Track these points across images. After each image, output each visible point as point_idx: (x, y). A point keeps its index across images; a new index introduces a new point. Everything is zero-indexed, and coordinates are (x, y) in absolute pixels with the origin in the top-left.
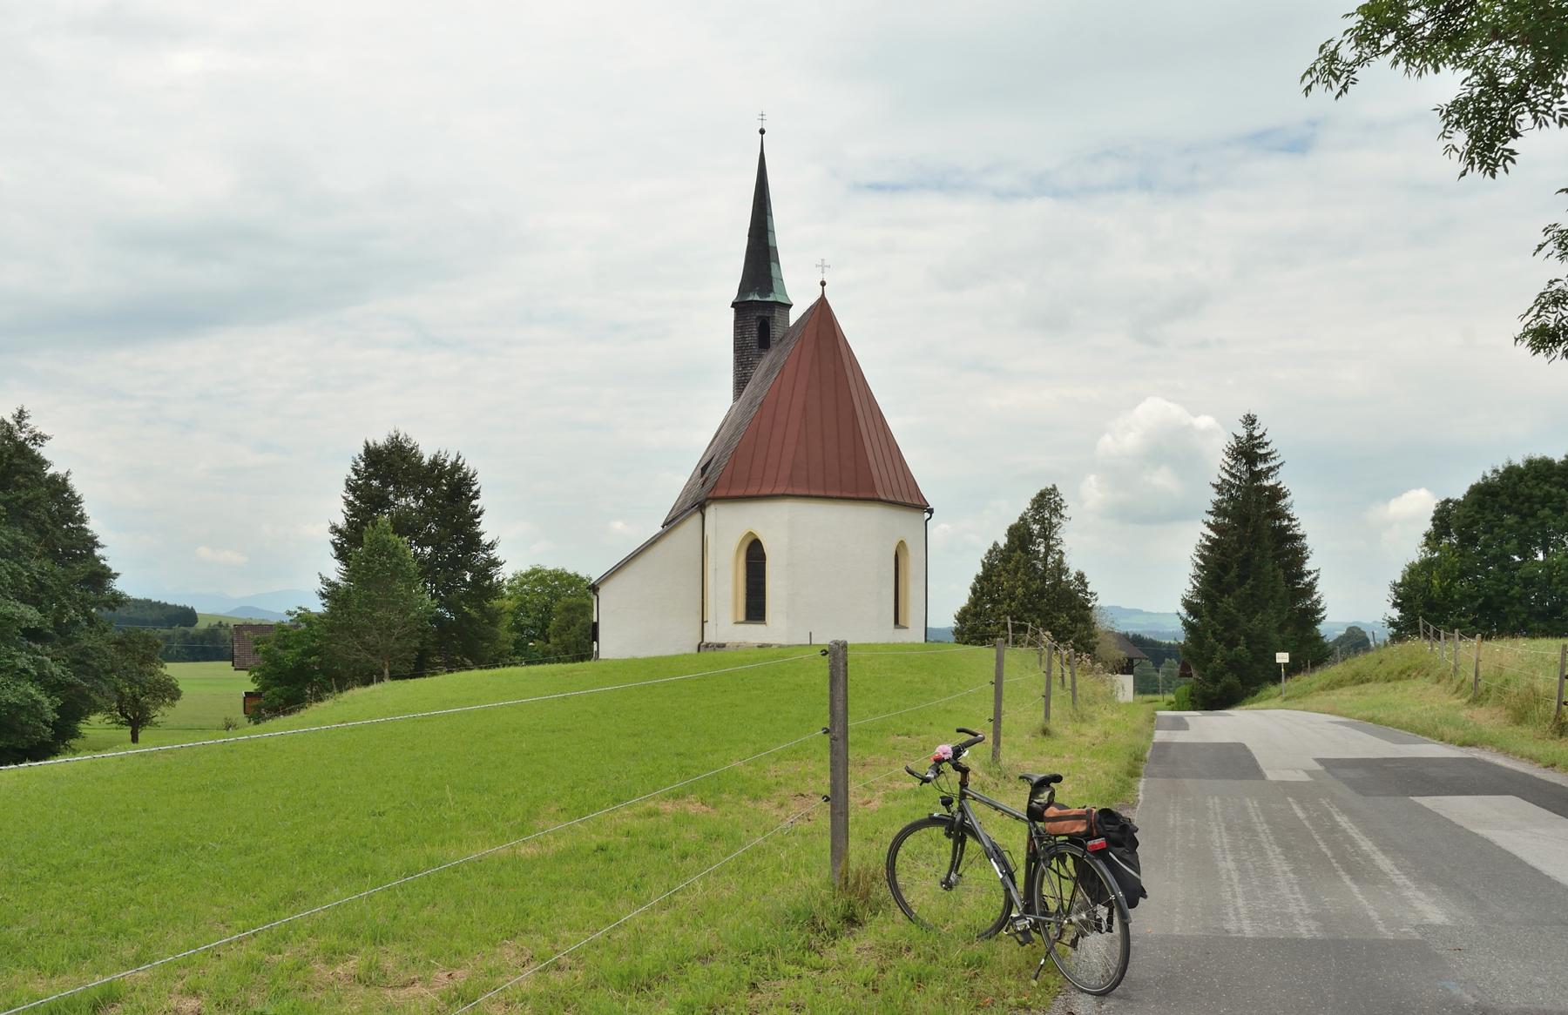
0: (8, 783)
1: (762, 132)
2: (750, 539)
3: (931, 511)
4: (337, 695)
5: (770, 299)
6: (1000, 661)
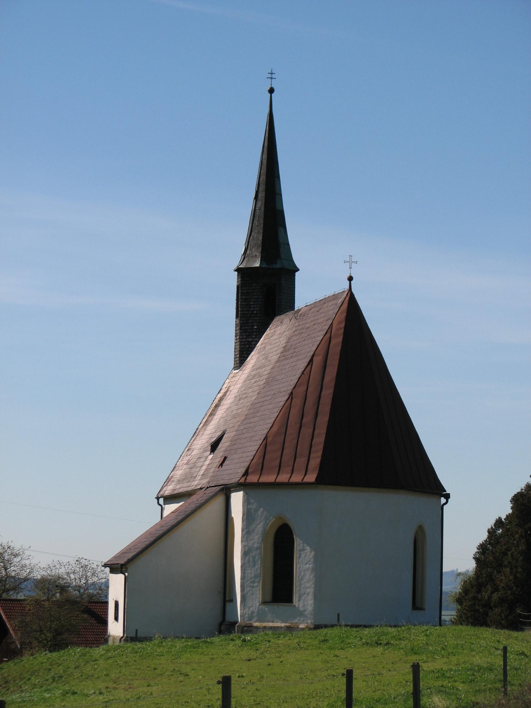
0: (496, 676)
1: (271, 91)
2: (280, 523)
3: (447, 497)
4: (47, 652)
5: (278, 266)
6: (443, 615)
